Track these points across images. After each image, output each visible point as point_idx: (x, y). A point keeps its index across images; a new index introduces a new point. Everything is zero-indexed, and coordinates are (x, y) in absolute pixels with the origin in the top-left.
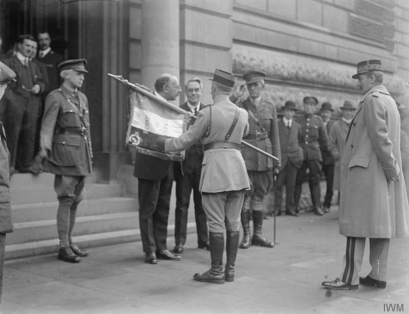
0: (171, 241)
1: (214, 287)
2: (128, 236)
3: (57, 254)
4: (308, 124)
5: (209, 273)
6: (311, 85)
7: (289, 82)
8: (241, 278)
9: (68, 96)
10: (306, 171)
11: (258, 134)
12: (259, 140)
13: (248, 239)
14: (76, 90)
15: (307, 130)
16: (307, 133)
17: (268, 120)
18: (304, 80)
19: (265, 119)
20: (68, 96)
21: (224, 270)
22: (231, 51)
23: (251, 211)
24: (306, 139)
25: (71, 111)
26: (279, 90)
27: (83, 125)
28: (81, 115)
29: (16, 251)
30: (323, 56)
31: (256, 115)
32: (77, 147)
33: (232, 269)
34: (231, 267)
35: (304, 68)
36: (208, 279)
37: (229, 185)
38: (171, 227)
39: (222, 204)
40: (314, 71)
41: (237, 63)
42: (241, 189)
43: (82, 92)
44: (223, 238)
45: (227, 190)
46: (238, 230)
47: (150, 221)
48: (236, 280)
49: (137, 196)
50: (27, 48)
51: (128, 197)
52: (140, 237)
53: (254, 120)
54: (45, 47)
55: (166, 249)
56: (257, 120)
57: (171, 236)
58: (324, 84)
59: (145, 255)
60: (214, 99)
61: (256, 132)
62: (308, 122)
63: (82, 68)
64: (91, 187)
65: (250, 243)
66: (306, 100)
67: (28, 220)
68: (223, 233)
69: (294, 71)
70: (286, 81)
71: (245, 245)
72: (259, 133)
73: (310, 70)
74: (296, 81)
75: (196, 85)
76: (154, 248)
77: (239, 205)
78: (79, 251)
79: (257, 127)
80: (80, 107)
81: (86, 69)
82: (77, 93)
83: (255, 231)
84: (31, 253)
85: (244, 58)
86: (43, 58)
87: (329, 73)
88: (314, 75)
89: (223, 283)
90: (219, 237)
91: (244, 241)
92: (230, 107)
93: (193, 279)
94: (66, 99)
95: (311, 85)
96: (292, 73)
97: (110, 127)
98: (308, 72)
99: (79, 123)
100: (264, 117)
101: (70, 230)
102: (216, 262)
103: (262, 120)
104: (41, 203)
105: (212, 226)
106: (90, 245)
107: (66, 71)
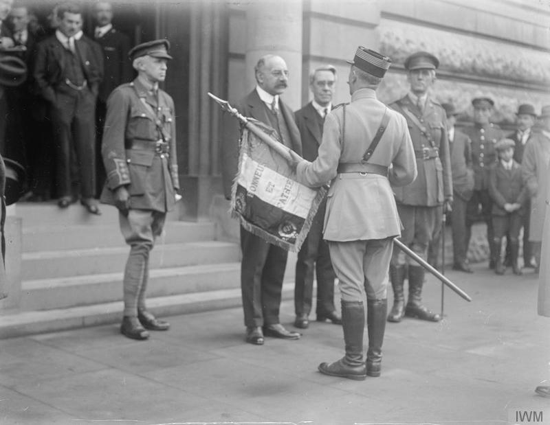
0: (287, 309)
1: (352, 385)
2: (224, 300)
3: (119, 326)
4: (483, 138)
5: (342, 364)
6: (494, 80)
7: (462, 75)
8: (392, 372)
9: (142, 94)
10: (477, 215)
11: (427, 151)
12: (427, 160)
13: (401, 309)
14: (156, 87)
15: (482, 147)
16: (481, 151)
17: (438, 128)
18: (485, 73)
19: (434, 128)
20: (142, 94)
21: (365, 358)
22: (379, 28)
23: (407, 267)
24: (481, 159)
25: (144, 115)
26: (447, 87)
27: (161, 136)
28: (159, 122)
29: (57, 320)
30: (513, 38)
31: (422, 121)
32: (148, 167)
33: (378, 357)
34: (376, 354)
35: (484, 56)
36: (342, 372)
37: (366, 231)
38: (289, 286)
39: (359, 256)
40: (499, 60)
41: (387, 47)
42: (386, 237)
43: (166, 91)
44: (362, 310)
45: (362, 239)
46: (385, 298)
47: (257, 281)
48: (383, 374)
49: (239, 241)
50: (69, 25)
51: (223, 241)
52: (241, 302)
53: (420, 130)
54: (104, 22)
55: (278, 323)
56: (423, 129)
57: (287, 299)
58: (512, 79)
59: (247, 330)
60: (351, 94)
61: (422, 148)
62: (481, 134)
63: (163, 52)
64: (170, 226)
65: (404, 313)
66: (475, 102)
67: (78, 274)
68: (362, 302)
69: (470, 60)
70: (457, 75)
71: (396, 317)
72: (427, 149)
73: (494, 59)
74: (471, 74)
75: (328, 76)
76: (260, 318)
77: (385, 258)
78: (156, 323)
79: (423, 139)
80: (158, 111)
81: (168, 54)
82: (157, 91)
83: (411, 297)
84: (79, 323)
85: (398, 39)
86: (101, 39)
87: (520, 63)
88: (499, 66)
89: (363, 379)
90: (355, 308)
91: (395, 311)
92: (376, 109)
93: (317, 370)
94: (139, 98)
95: (494, 80)
96: (467, 62)
97: (199, 139)
98: (490, 61)
99: (153, 134)
100: (433, 124)
101: (143, 290)
102: (352, 345)
103: (431, 128)
104: (97, 249)
105: (344, 290)
106: (166, 313)
107: (141, 58)
